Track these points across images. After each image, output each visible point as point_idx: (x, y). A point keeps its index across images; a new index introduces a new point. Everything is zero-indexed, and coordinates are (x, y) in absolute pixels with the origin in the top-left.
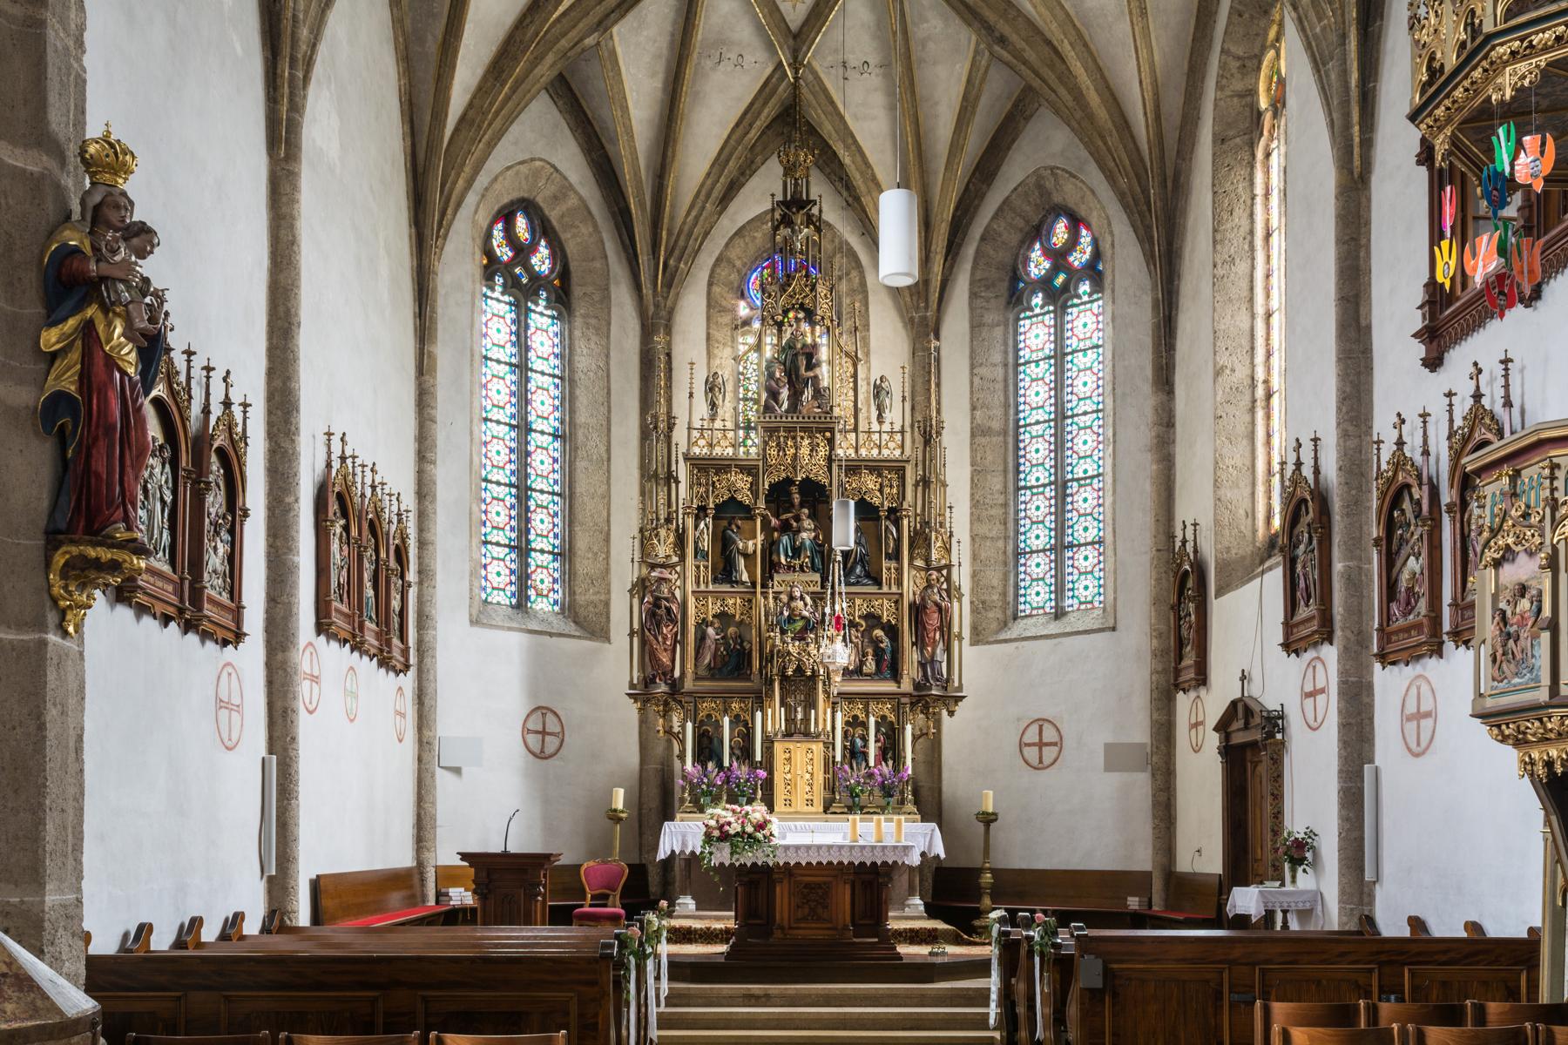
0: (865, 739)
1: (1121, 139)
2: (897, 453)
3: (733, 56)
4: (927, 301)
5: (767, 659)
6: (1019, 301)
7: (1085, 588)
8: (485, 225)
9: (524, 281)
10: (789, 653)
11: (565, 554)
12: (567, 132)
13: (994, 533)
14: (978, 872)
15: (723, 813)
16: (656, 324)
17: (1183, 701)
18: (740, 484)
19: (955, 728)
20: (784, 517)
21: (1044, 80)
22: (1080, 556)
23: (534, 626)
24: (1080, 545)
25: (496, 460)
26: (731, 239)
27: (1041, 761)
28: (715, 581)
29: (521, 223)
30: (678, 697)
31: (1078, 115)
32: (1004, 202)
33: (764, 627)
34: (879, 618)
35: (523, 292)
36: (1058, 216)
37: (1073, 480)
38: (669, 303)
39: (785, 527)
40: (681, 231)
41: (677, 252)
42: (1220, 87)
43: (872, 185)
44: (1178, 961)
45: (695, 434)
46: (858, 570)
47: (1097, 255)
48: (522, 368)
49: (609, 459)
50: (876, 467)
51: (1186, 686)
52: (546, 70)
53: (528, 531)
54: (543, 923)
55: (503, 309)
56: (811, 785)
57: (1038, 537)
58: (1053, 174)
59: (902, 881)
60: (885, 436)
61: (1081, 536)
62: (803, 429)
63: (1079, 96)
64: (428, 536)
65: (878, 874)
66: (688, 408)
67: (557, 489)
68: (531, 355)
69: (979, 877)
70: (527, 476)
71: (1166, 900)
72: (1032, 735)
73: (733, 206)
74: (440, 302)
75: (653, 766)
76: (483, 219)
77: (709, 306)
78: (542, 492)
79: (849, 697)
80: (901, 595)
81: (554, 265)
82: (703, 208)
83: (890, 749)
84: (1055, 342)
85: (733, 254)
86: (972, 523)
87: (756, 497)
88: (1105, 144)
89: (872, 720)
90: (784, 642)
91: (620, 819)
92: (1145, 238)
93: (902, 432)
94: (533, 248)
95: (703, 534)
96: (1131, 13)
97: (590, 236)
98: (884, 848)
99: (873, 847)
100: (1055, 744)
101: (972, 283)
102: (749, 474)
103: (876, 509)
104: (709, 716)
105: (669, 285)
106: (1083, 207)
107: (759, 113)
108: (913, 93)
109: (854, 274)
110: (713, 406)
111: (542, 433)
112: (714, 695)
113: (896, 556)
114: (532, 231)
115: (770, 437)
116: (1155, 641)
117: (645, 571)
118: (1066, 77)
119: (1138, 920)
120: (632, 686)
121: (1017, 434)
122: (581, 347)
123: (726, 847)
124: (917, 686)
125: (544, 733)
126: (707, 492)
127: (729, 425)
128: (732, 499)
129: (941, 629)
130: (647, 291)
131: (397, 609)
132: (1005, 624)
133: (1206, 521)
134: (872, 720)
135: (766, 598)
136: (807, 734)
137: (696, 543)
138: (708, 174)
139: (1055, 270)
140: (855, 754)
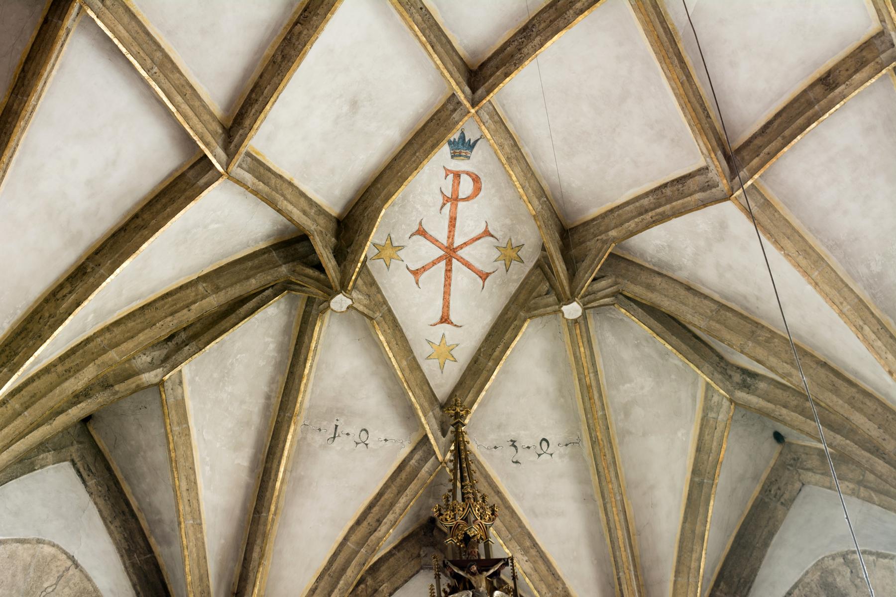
3: (354, 430)
107: (392, 505)
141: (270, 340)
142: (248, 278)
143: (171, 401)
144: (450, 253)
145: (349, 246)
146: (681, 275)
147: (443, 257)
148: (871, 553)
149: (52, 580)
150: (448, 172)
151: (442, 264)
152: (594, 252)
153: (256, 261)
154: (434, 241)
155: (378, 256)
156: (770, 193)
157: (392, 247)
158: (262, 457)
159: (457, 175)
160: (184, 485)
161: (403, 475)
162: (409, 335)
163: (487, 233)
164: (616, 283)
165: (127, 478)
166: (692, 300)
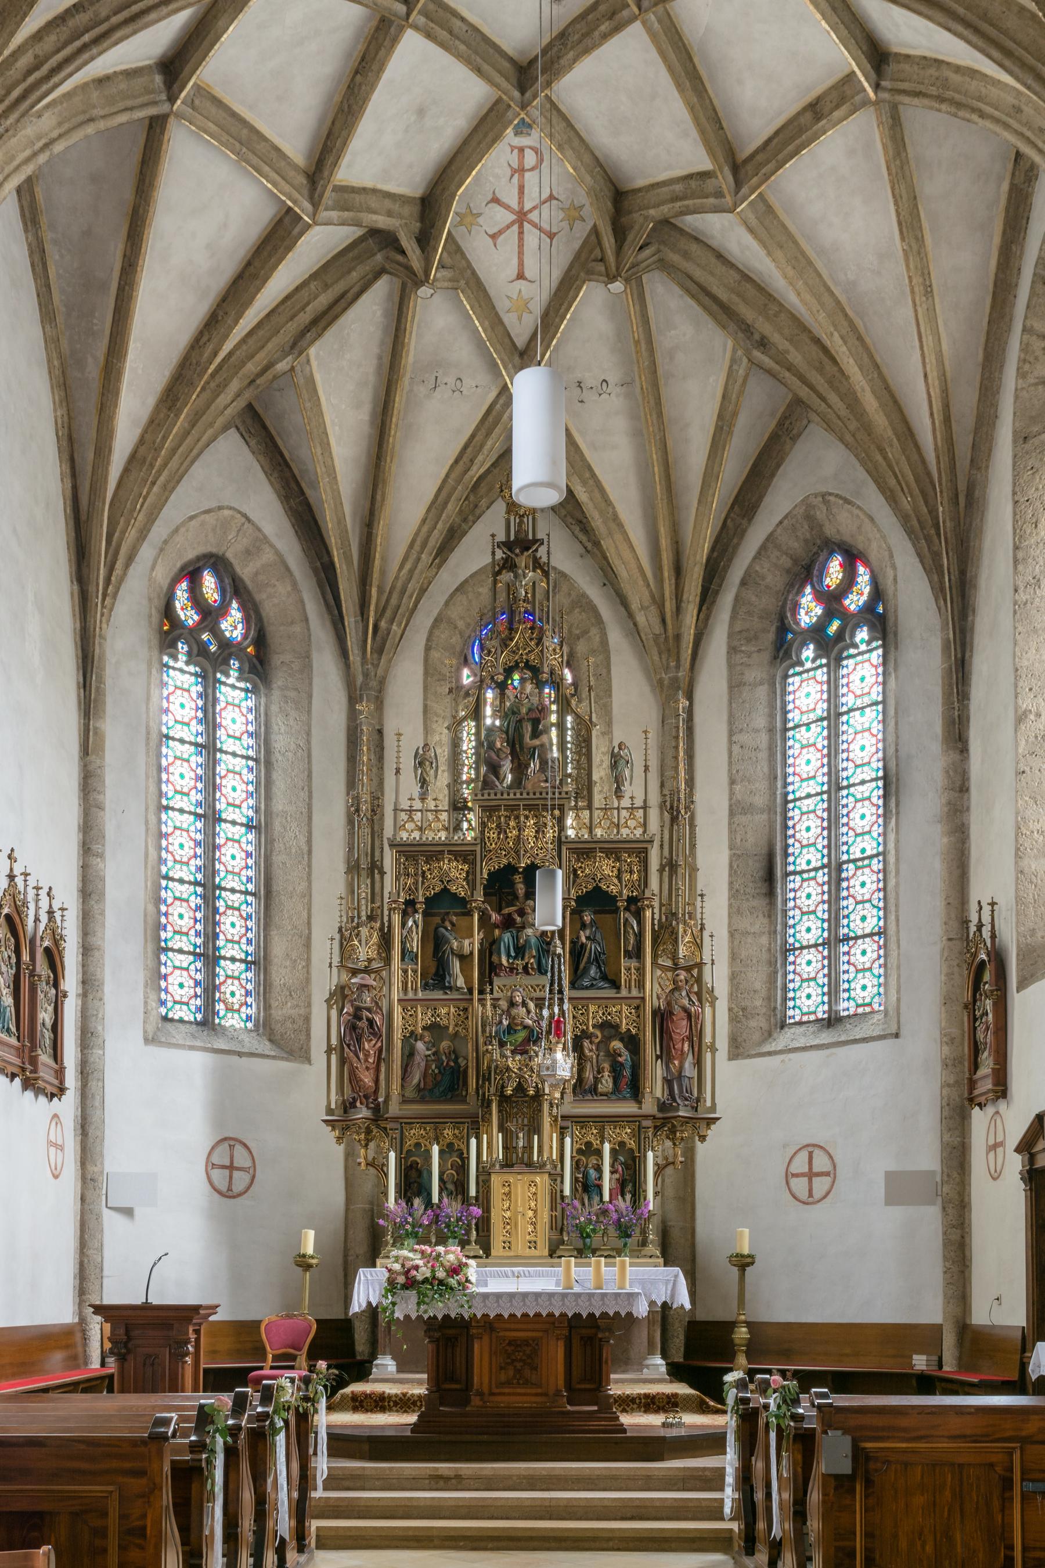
0: (599, 1169)
1: (904, 451)
2: (638, 832)
3: (451, 380)
4: (678, 660)
5: (484, 1077)
6: (787, 655)
7: (863, 989)
8: (165, 583)
9: (213, 648)
10: (508, 1069)
11: (259, 963)
12: (261, 475)
13: (756, 928)
14: (729, 1326)
15: (409, 1255)
16: (365, 692)
17: (979, 1118)
18: (454, 873)
19: (712, 1153)
20: (506, 911)
21: (811, 387)
22: (857, 950)
23: (221, 1044)
24: (856, 938)
25: (179, 854)
26: (452, 596)
27: (811, 1195)
28: (425, 987)
29: (209, 583)
30: (383, 1124)
31: (853, 425)
32: (767, 539)
33: (481, 1040)
34: (617, 1027)
35: (211, 662)
36: (831, 553)
37: (849, 861)
38: (380, 672)
39: (508, 923)
40: (393, 588)
41: (388, 613)
42: (1021, 374)
43: (613, 526)
44: (953, 1438)
45: (403, 816)
46: (593, 971)
47: (877, 594)
48: (209, 749)
49: (310, 852)
50: (613, 850)
51: (982, 1099)
52: (229, 401)
53: (216, 936)
54: (195, 1389)
55: (187, 680)
56: (534, 1224)
57: (808, 929)
58: (826, 502)
59: (641, 1337)
60: (624, 813)
61: (858, 927)
62: (527, 807)
63: (853, 402)
64: (93, 940)
65: (598, 1327)
66: (401, 788)
67: (251, 887)
68: (221, 733)
69: (732, 1332)
70: (214, 872)
71: (960, 1359)
72: (800, 1164)
73: (455, 557)
74: (109, 671)
75: (360, 1206)
76: (162, 576)
77: (426, 673)
78: (233, 891)
79: (582, 1121)
80: (643, 999)
81: (248, 629)
82: (419, 559)
83: (630, 1180)
84: (829, 700)
85: (454, 613)
86: (730, 916)
87: (473, 888)
88: (885, 458)
89: (607, 1147)
90: (503, 1056)
91: (309, 1267)
92: (932, 566)
93: (645, 807)
94: (223, 610)
95: (410, 933)
96: (913, 292)
97: (290, 594)
98: (604, 1295)
99: (591, 1295)
100: (827, 1174)
101: (731, 635)
102: (465, 861)
103: (611, 899)
104: (418, 1145)
105: (380, 651)
106: (861, 538)
107: (482, 446)
108: (660, 415)
109: (594, 631)
110: (423, 782)
111: (234, 823)
112: (423, 1120)
113: (637, 953)
114: (223, 592)
115: (490, 817)
116: (946, 1048)
117: (345, 977)
118: (838, 378)
119: (926, 1384)
120: (329, 1111)
121: (785, 811)
122: (279, 724)
123: (412, 1295)
124: (662, 1107)
125: (231, 1168)
126: (416, 883)
127: (444, 805)
128: (445, 890)
129: (690, 1039)
130: (355, 657)
131: (49, 1023)
132: (770, 1035)
133: (1006, 900)
134: (607, 1147)
135: (484, 1006)
136: (530, 1164)
137: (403, 943)
138: (424, 521)
139: (829, 615)
140: (587, 1187)
141: (375, 308)
142: (349, 272)
143: (302, 381)
144: (522, 217)
145: (433, 226)
146: (714, 244)
147: (516, 224)
148: (841, 498)
149: (233, 534)
150: (513, 148)
151: (516, 227)
152: (637, 227)
153: (356, 251)
154: (507, 207)
155: (461, 223)
156: (772, 199)
157: (469, 217)
158: (380, 410)
159: (521, 150)
160: (319, 451)
161: (490, 419)
162: (492, 292)
163: (551, 197)
164: (659, 251)
165: (279, 434)
166: (721, 269)
